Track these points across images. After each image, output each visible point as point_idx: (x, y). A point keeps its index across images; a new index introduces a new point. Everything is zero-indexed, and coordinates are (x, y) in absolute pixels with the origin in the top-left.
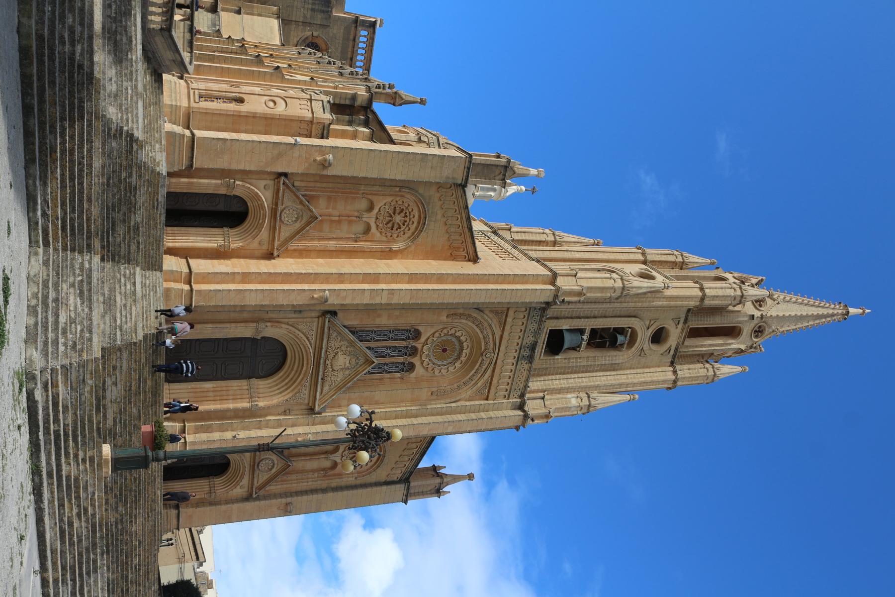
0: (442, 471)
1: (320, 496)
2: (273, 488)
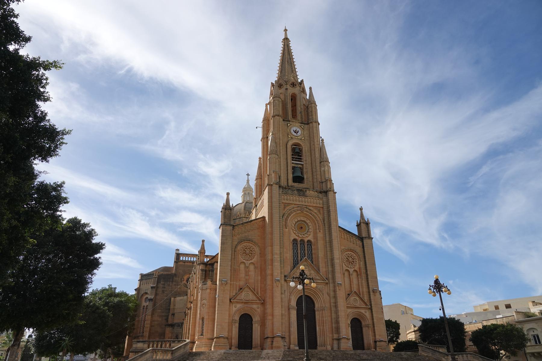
1: (369, 277)
2: (366, 299)
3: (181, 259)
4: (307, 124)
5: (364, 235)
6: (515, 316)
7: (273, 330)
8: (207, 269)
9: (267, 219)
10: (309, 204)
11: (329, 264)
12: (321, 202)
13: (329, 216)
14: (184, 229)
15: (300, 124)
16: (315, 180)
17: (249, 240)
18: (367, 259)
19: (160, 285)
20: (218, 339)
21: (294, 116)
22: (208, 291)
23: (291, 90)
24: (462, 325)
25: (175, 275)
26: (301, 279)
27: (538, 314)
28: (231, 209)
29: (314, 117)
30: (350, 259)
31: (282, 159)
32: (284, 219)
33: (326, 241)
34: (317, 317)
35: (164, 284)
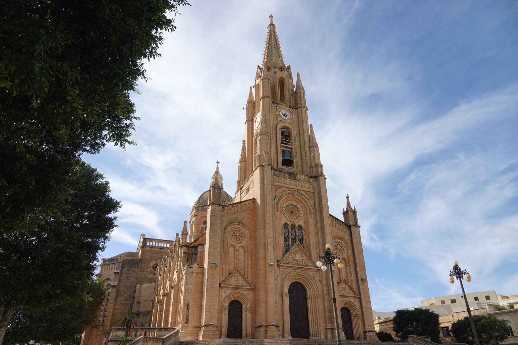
0: (345, 210)
1: (357, 265)
2: (355, 287)
3: (148, 244)
4: (296, 109)
5: (352, 223)
6: (487, 308)
7: (266, 318)
8: (190, 252)
9: (258, 201)
10: (300, 188)
12: (312, 186)
13: (320, 201)
14: (130, 220)
15: (288, 108)
16: (304, 165)
17: (239, 222)
18: (355, 247)
19: (125, 271)
20: (207, 328)
21: (283, 99)
22: (194, 274)
23: (279, 74)
24: (437, 316)
25: (141, 260)
26: (328, 259)
27: (506, 307)
28: (220, 189)
29: (303, 102)
30: (339, 247)
31: (272, 140)
32: (276, 201)
33: (317, 226)
34: (309, 305)
35: (129, 270)
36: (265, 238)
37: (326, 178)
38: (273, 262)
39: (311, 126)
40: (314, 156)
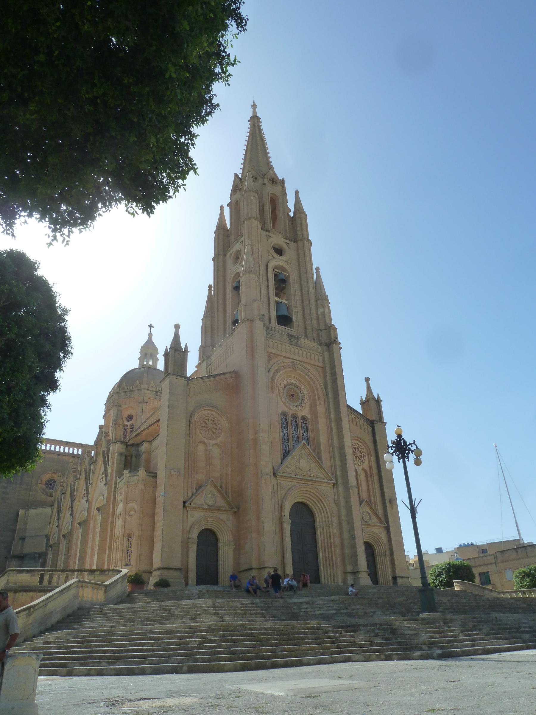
0: (364, 399)
11: (337, 455)
23: (270, 189)
29: (305, 232)
33: (330, 419)
36: (256, 432)
37: (341, 348)
38: (268, 470)
39: (318, 269)
40: (323, 314)
